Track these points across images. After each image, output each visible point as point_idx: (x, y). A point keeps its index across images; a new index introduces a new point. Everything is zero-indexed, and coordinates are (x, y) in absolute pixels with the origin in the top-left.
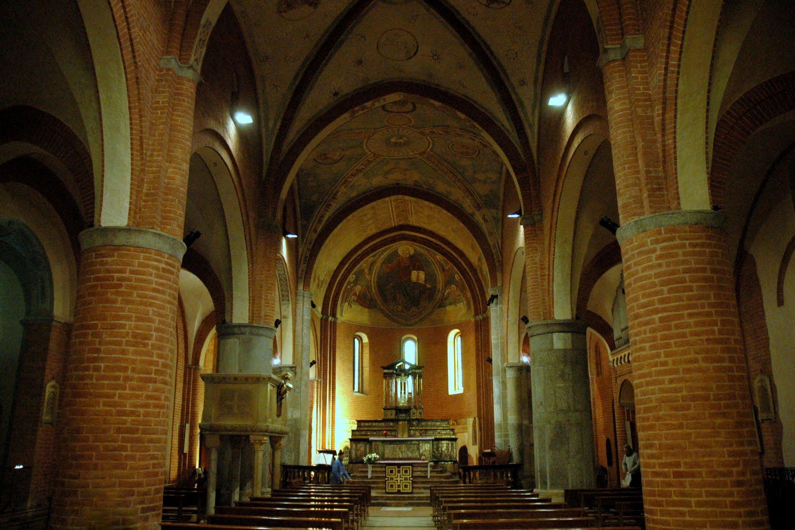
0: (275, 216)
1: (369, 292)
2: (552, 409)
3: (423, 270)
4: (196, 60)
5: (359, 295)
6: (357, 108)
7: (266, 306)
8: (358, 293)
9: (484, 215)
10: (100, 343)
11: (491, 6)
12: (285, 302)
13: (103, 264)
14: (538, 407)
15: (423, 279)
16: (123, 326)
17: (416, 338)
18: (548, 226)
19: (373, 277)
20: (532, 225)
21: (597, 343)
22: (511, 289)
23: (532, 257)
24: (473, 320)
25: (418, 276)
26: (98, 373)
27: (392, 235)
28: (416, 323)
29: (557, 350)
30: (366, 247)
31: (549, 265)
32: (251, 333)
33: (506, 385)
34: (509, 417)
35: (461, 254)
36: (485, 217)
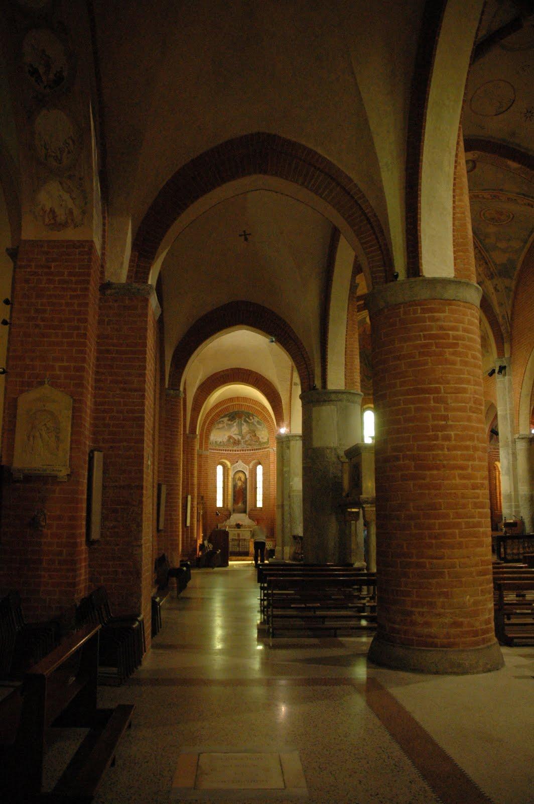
9: (497, 285)
10: (446, 409)
13: (432, 319)
16: (464, 391)
17: (372, 406)
22: (530, 360)
26: (448, 442)
32: (348, 401)
33: (516, 457)
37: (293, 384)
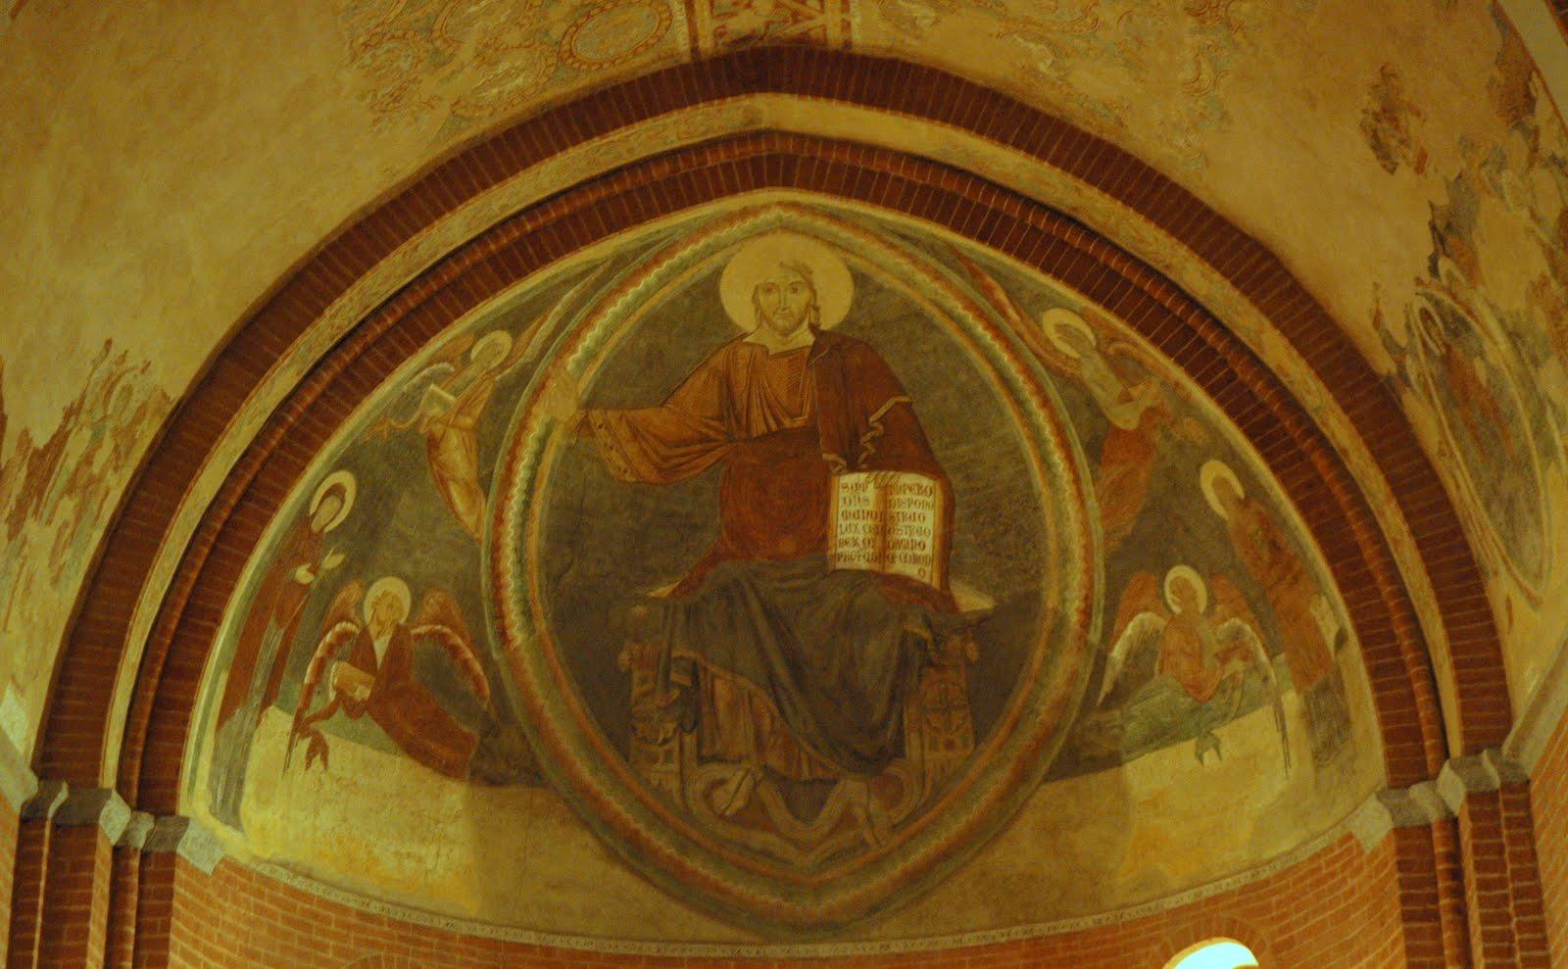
1: (478, 643)
3: (926, 463)
5: (396, 650)
8: (381, 647)
15: (929, 545)
19: (512, 515)
24: (1374, 826)
25: (884, 525)
28: (873, 910)
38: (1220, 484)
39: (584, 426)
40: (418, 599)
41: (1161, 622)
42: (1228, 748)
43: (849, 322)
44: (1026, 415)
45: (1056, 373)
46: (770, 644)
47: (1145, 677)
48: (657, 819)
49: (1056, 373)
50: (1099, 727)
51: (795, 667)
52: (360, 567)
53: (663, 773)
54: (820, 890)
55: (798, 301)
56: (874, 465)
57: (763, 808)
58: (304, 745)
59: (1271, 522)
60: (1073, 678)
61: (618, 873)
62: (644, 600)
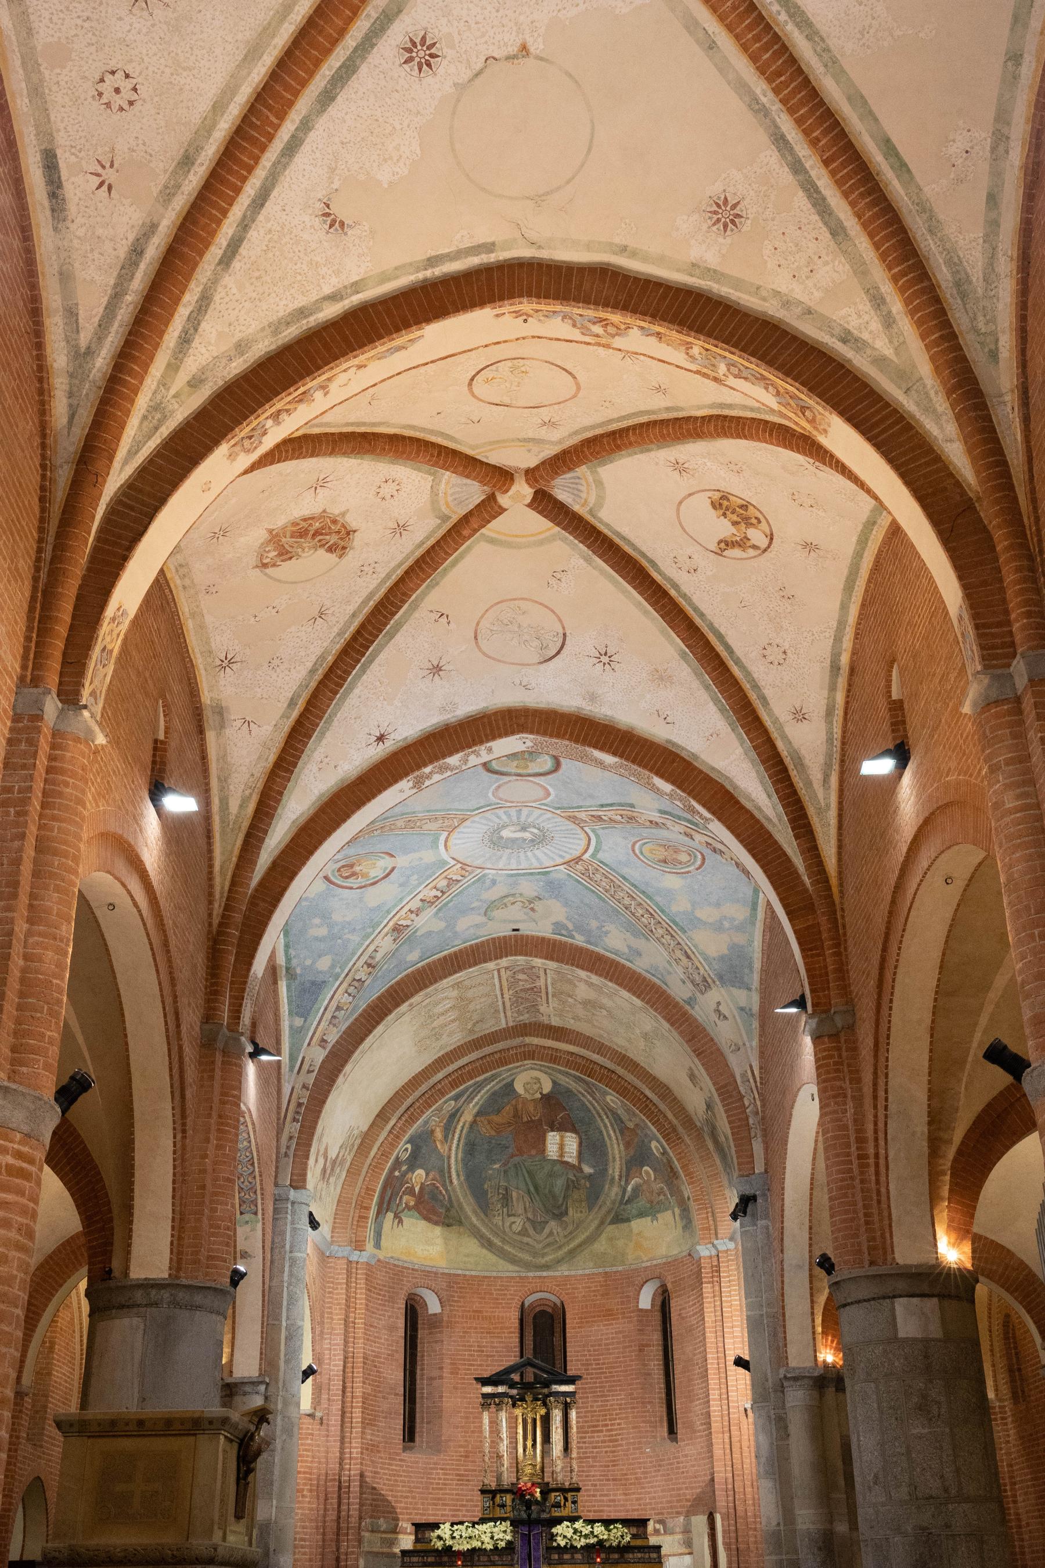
0: (239, 1018)
1: (444, 1185)
2: (903, 1492)
3: (574, 1130)
4: (93, 694)
6: (427, 770)
7: (213, 1235)
8: (417, 1189)
11: (725, 553)
12: (247, 1217)
14: (870, 1489)
18: (870, 1041)
19: (454, 1148)
20: (830, 1036)
21: (1007, 1316)
23: (835, 1112)
25: (562, 1147)
27: (501, 1045)
28: (559, 1261)
29: (906, 1340)
30: (440, 1075)
31: (876, 1132)
32: (175, 1304)
33: (786, 1427)
34: (798, 1512)
35: (664, 1091)
36: (721, 1008)
37: (238, 1255)
38: (656, 1147)
39: (474, 1122)
40: (427, 1174)
41: (641, 1181)
42: (660, 1221)
43: (551, 1092)
44: (602, 1120)
45: (610, 1110)
46: (528, 1179)
47: (637, 1197)
48: (496, 1234)
49: (610, 1110)
50: (624, 1210)
51: (536, 1188)
52: (412, 1168)
53: (498, 1220)
54: (543, 1255)
55: (536, 1087)
56: (559, 1130)
57: (526, 1230)
58: (397, 1221)
59: (670, 1161)
60: (616, 1195)
61: (485, 1251)
62: (492, 1169)
